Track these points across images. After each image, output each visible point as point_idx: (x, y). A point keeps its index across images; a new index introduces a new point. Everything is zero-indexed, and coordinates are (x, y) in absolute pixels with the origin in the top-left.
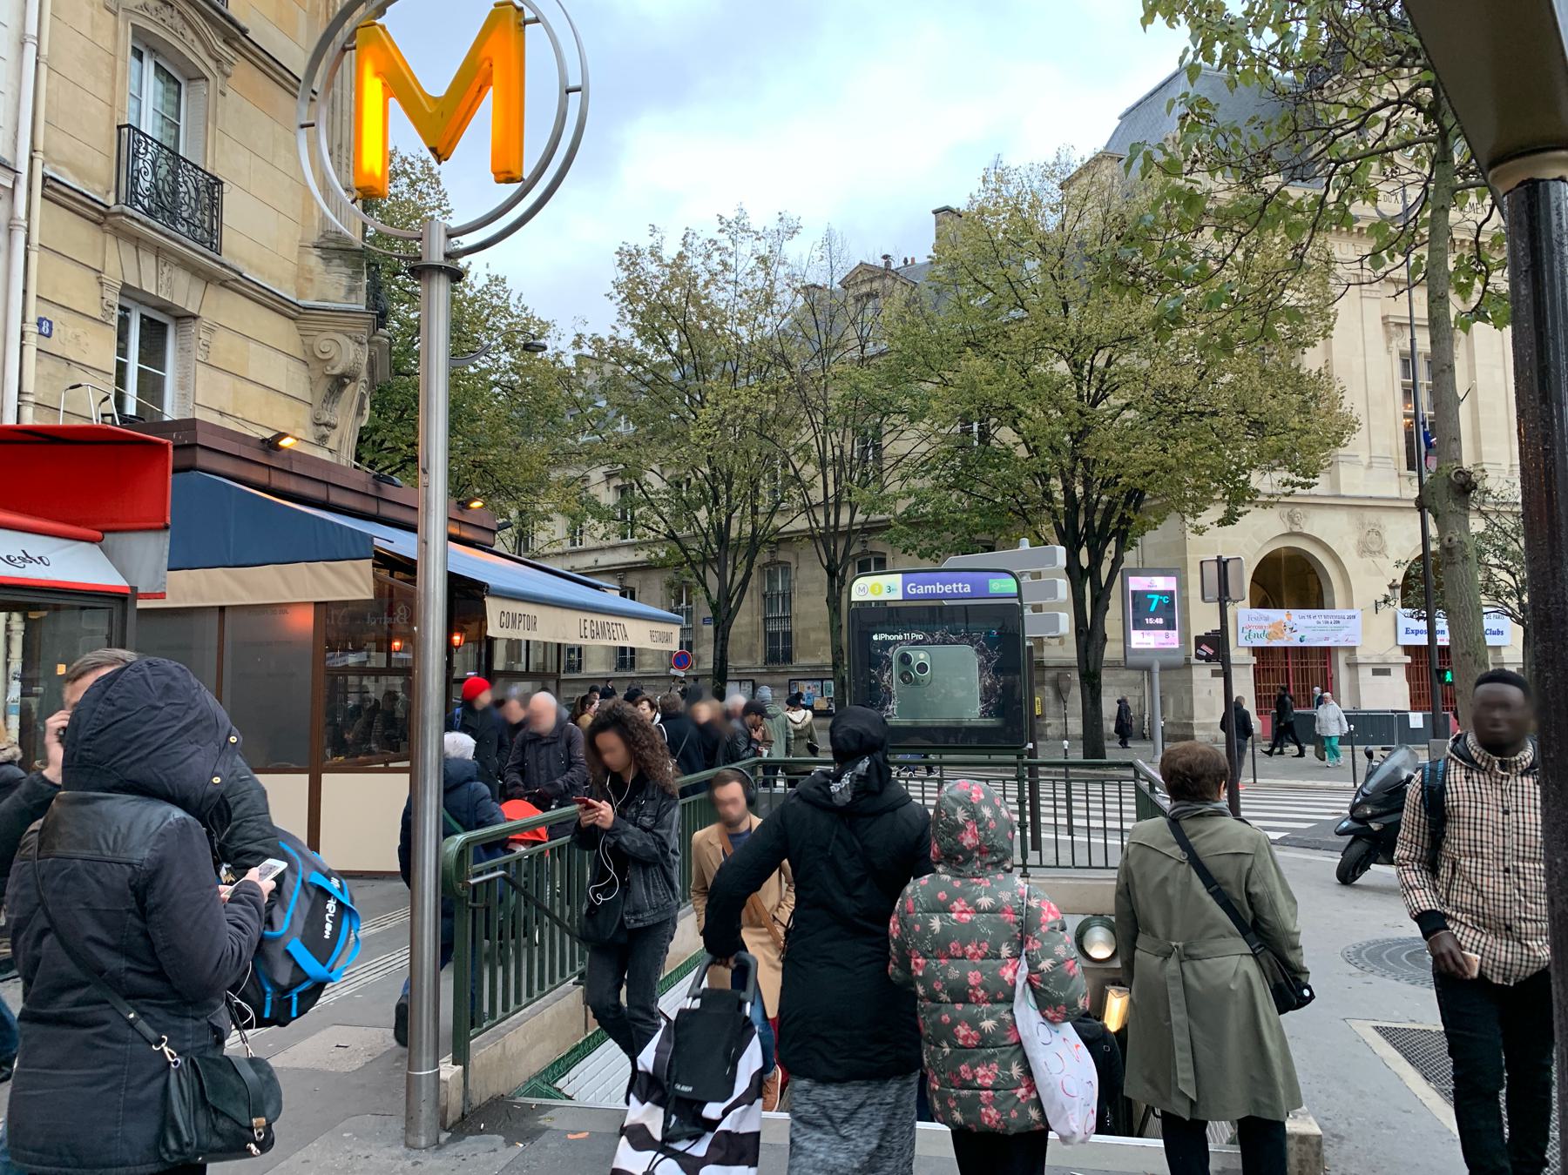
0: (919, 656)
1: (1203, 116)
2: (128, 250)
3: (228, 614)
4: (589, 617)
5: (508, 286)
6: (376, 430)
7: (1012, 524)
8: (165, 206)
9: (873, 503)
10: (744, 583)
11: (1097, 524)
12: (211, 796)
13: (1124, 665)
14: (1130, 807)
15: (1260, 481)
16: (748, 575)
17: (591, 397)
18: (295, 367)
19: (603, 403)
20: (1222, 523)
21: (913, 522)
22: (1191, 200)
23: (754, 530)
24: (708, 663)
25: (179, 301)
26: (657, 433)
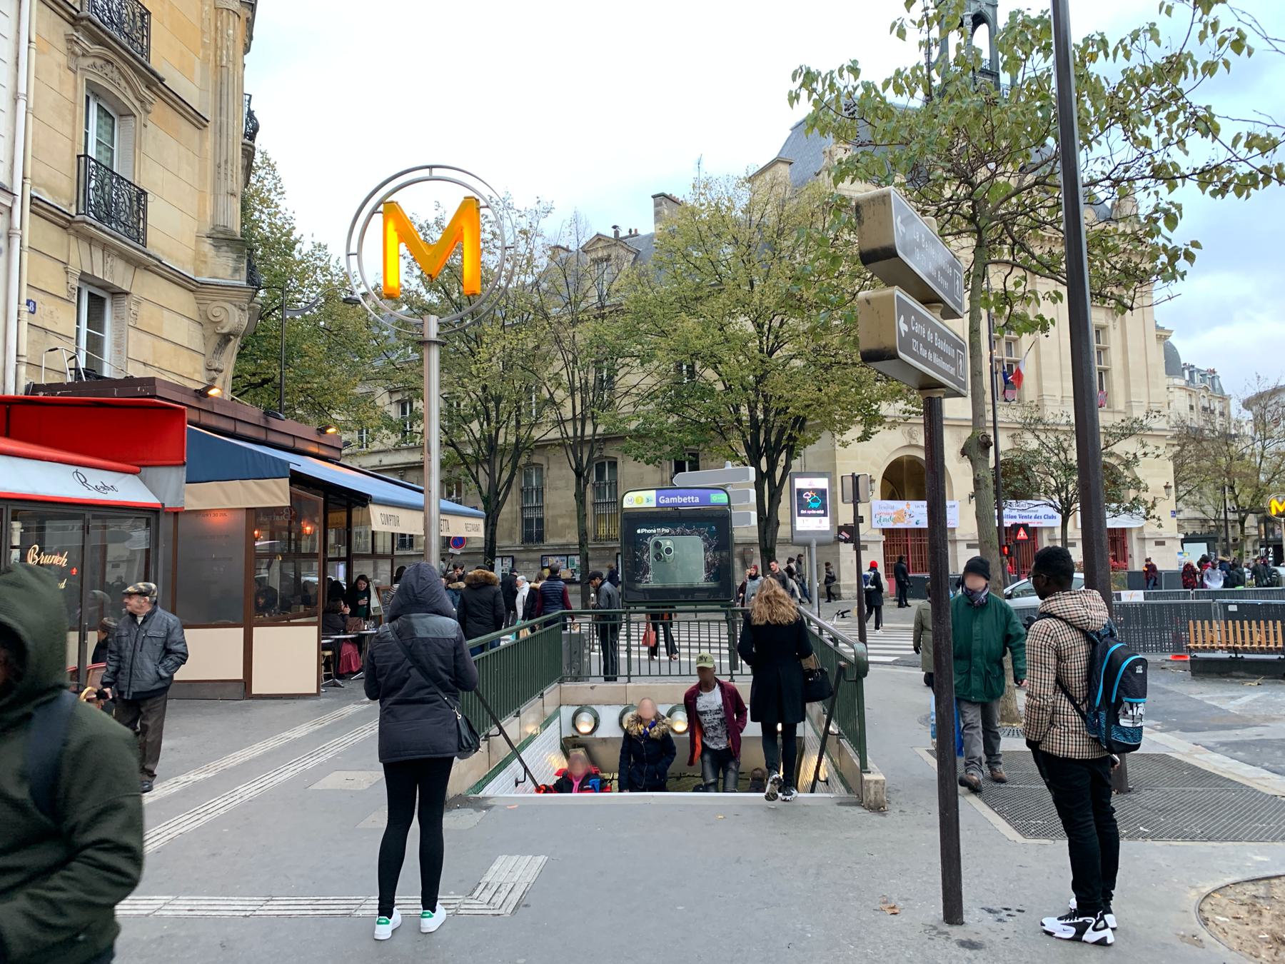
0: (667, 543)
2: (84, 246)
8: (107, 213)
10: (509, 482)
11: (773, 439)
13: (791, 542)
15: (886, 409)
18: (195, 328)
20: (861, 439)
21: (639, 435)
25: (117, 284)
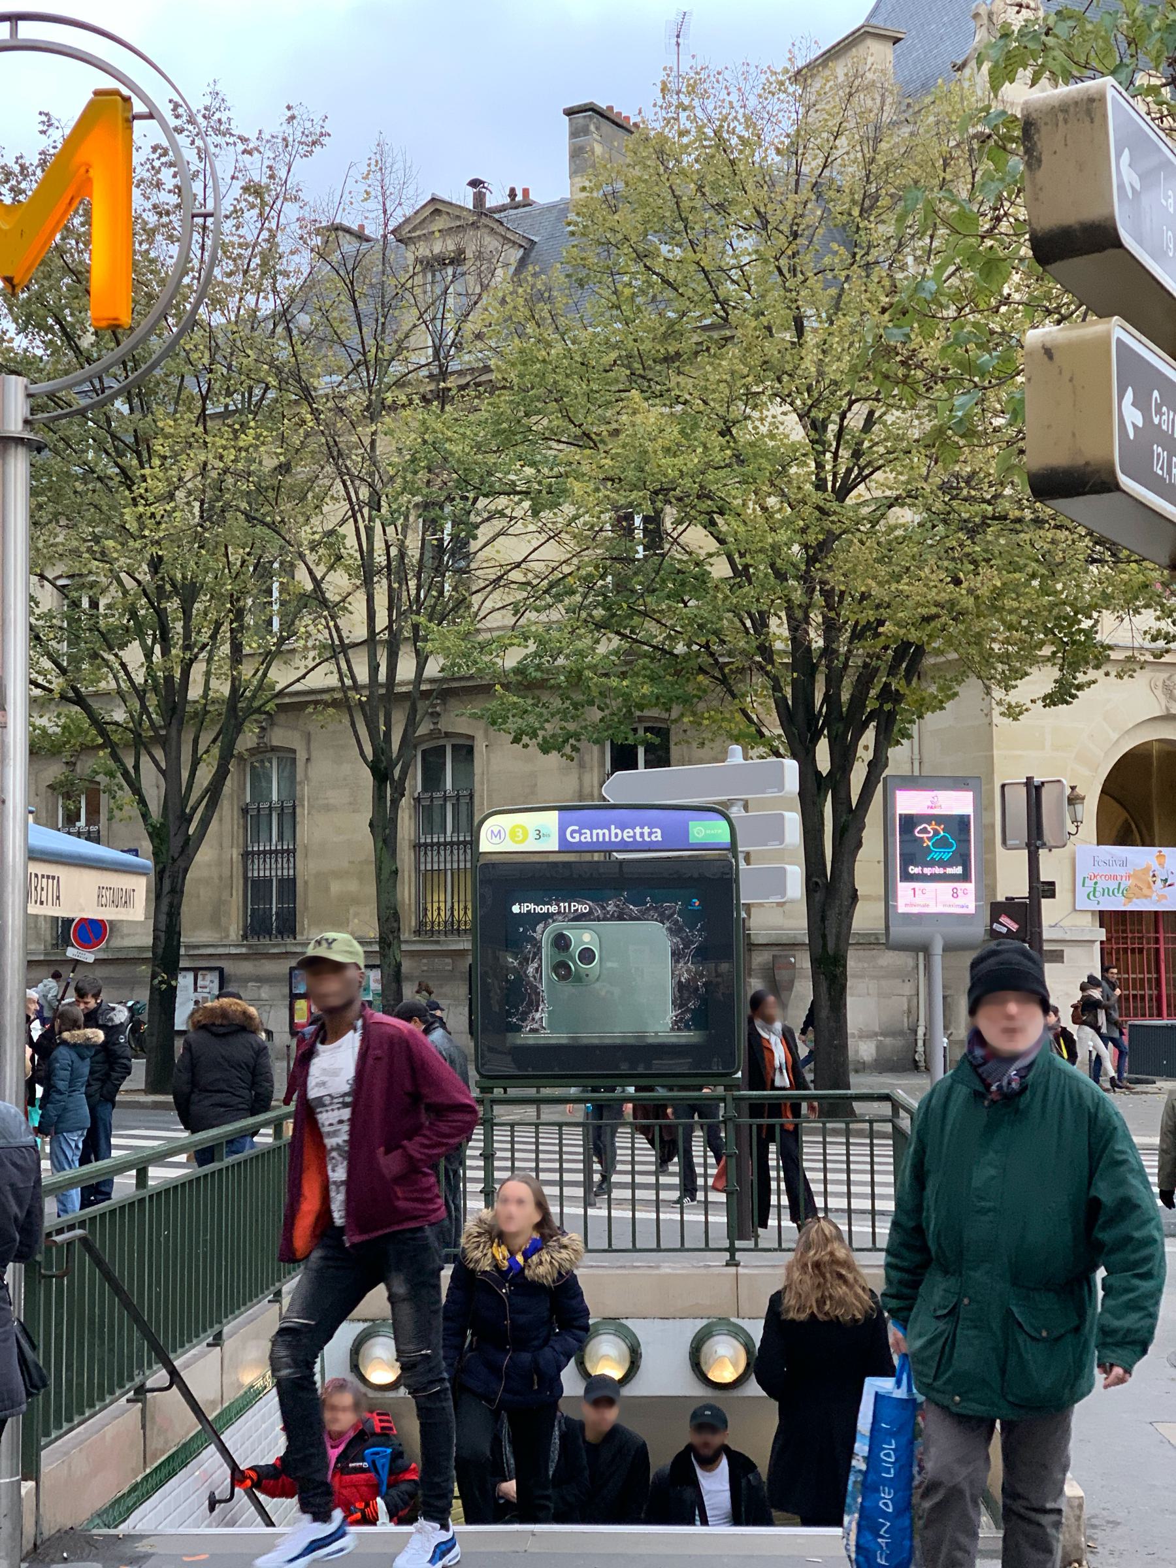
0: (584, 937)
11: (845, 696)
13: (884, 941)
15: (1115, 629)
20: (1051, 700)
21: (525, 682)
23: (234, 690)
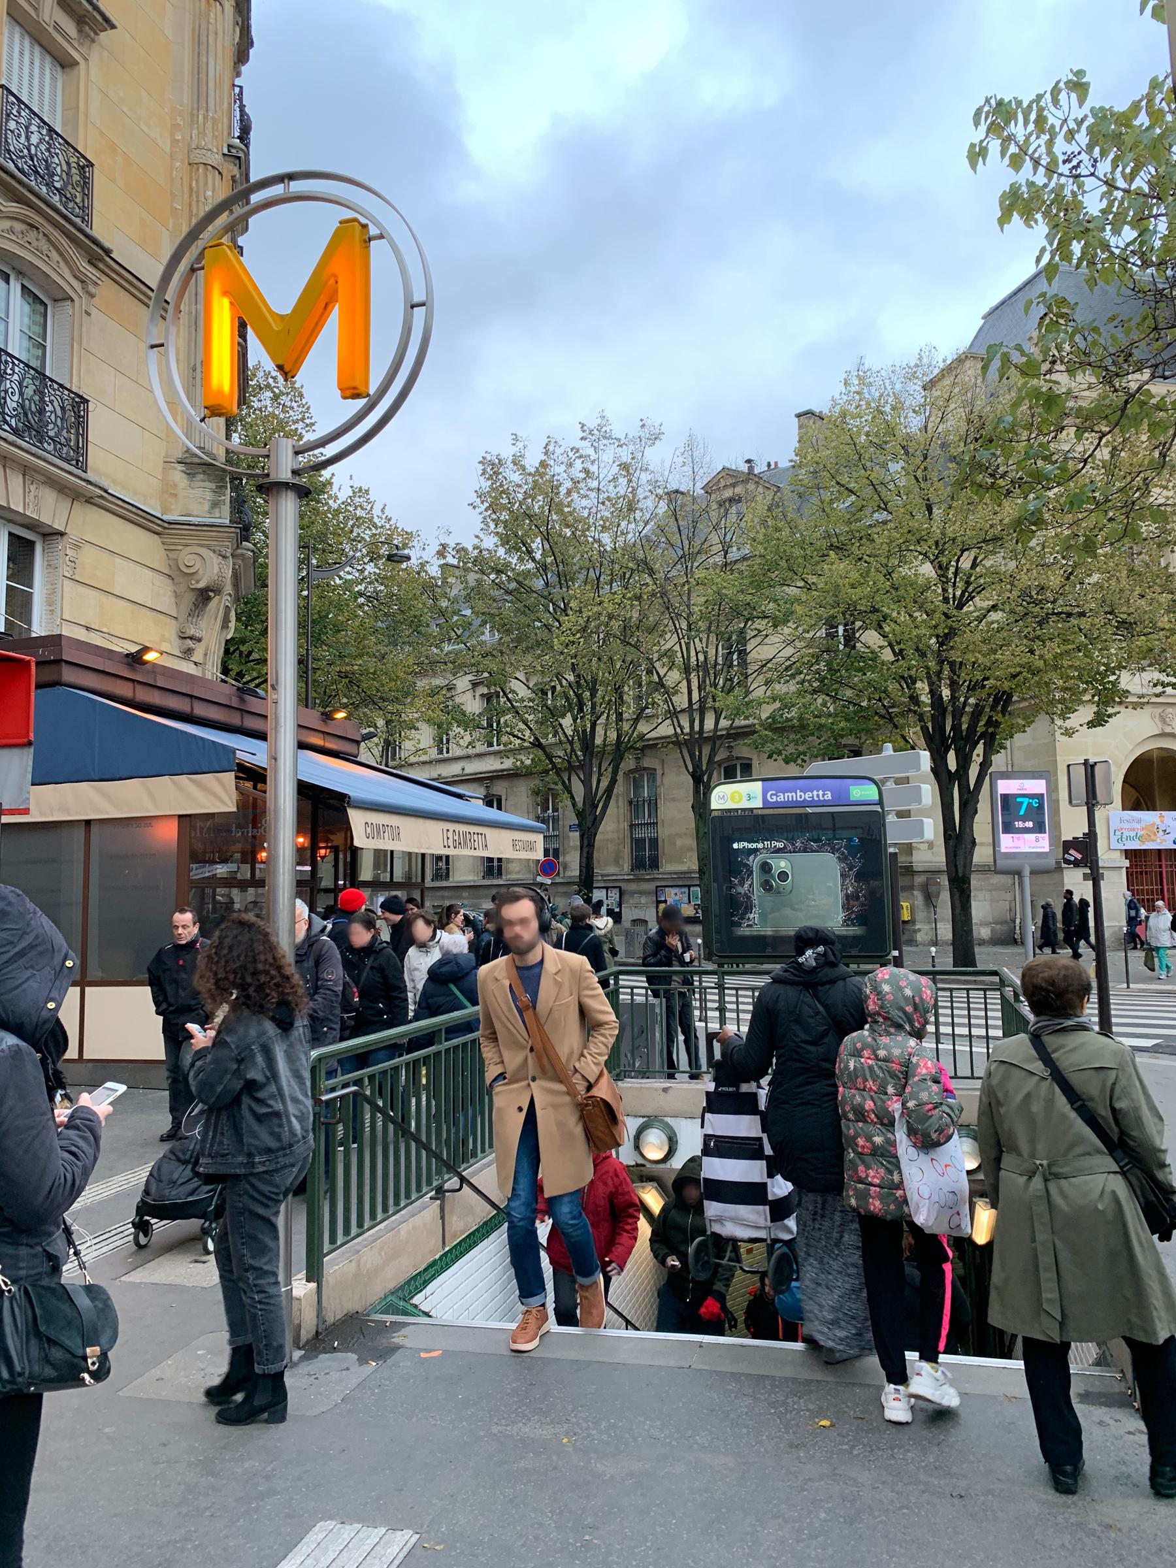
0: (781, 864)
1: (1062, 316)
3: (94, 829)
4: (451, 826)
5: (372, 497)
6: (243, 641)
7: (878, 727)
9: (738, 709)
11: (964, 726)
12: (45, 1022)
13: (993, 869)
14: (996, 1014)
15: (1128, 681)
16: (613, 782)
17: (456, 606)
18: (161, 581)
19: (468, 612)
20: (1092, 724)
21: (777, 727)
22: (1051, 400)
23: (619, 737)
24: (574, 871)
25: (45, 519)
26: (521, 642)
